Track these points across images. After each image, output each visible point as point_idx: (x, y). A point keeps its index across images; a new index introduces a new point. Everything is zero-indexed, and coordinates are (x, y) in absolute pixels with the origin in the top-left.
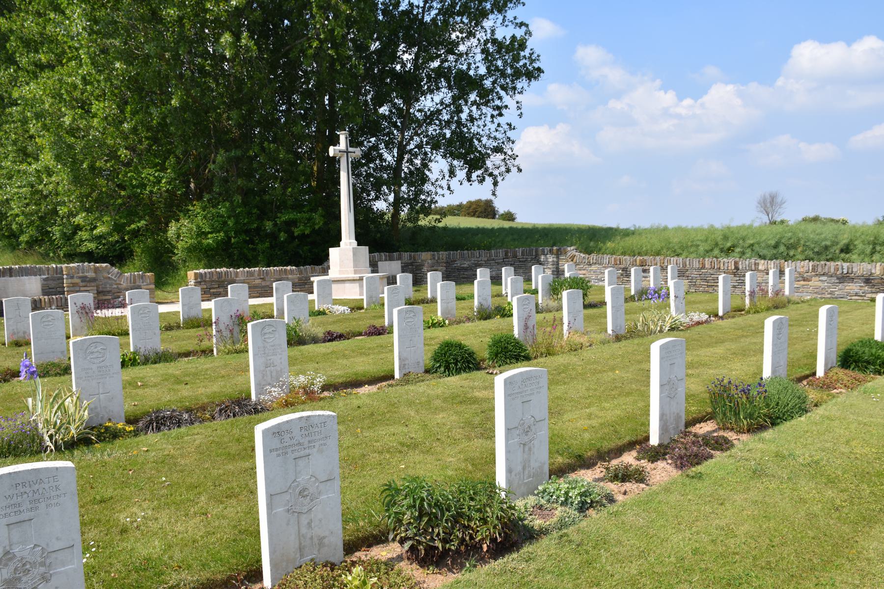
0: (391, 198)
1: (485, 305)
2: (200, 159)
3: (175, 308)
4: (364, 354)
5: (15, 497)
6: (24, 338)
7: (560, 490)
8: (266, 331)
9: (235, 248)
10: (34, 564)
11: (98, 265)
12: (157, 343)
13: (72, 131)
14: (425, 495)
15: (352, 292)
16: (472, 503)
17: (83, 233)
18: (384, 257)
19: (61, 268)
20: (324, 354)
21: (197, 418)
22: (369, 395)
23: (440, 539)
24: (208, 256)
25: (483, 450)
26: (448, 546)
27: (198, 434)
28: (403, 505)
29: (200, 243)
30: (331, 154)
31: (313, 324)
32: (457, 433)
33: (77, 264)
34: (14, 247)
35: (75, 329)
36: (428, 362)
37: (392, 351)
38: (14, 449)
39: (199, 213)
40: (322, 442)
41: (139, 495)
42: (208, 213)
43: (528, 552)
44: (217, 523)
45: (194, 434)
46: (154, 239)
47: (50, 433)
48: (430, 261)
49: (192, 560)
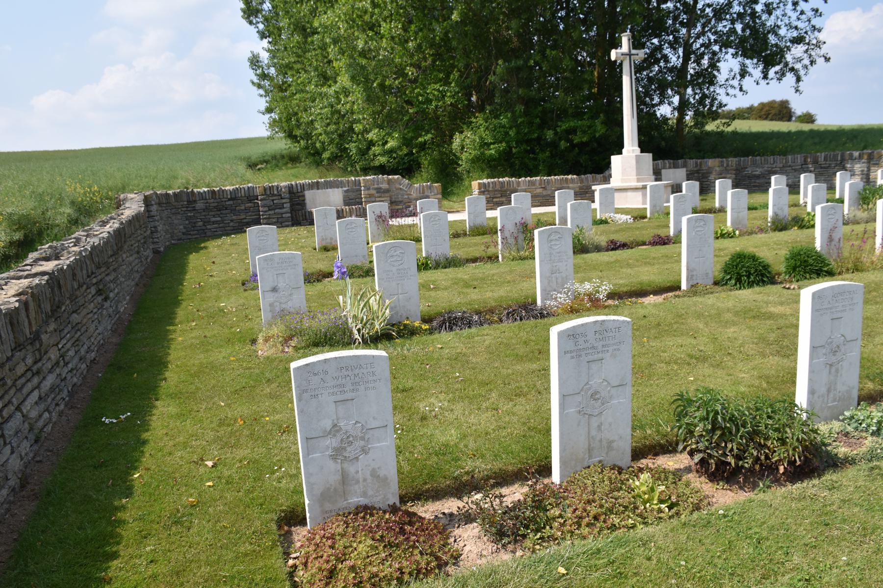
0: (676, 100)
1: (781, 214)
2: (481, 71)
3: (462, 217)
4: (649, 263)
5: (340, 379)
6: (331, 243)
7: (872, 419)
8: (552, 237)
9: (516, 158)
10: (355, 438)
11: (390, 177)
12: (446, 249)
13: (363, 54)
14: (719, 408)
15: (634, 201)
16: (770, 422)
17: (376, 148)
18: (668, 165)
19: (359, 180)
20: (608, 263)
21: (486, 320)
22: (655, 305)
23: (733, 455)
24: (490, 167)
25: (779, 368)
26: (741, 463)
27: (487, 335)
28: (696, 417)
29: (483, 153)
30: (613, 58)
31: (596, 234)
32: (750, 348)
33: (372, 177)
34: (318, 164)
35: (373, 236)
36: (717, 273)
37: (679, 261)
38: (330, 340)
39: (481, 125)
40: (616, 347)
41: (436, 388)
42: (490, 124)
43: (831, 480)
44: (507, 419)
45: (483, 335)
46: (440, 151)
47: (358, 327)
48: (718, 169)
49: (485, 450)
